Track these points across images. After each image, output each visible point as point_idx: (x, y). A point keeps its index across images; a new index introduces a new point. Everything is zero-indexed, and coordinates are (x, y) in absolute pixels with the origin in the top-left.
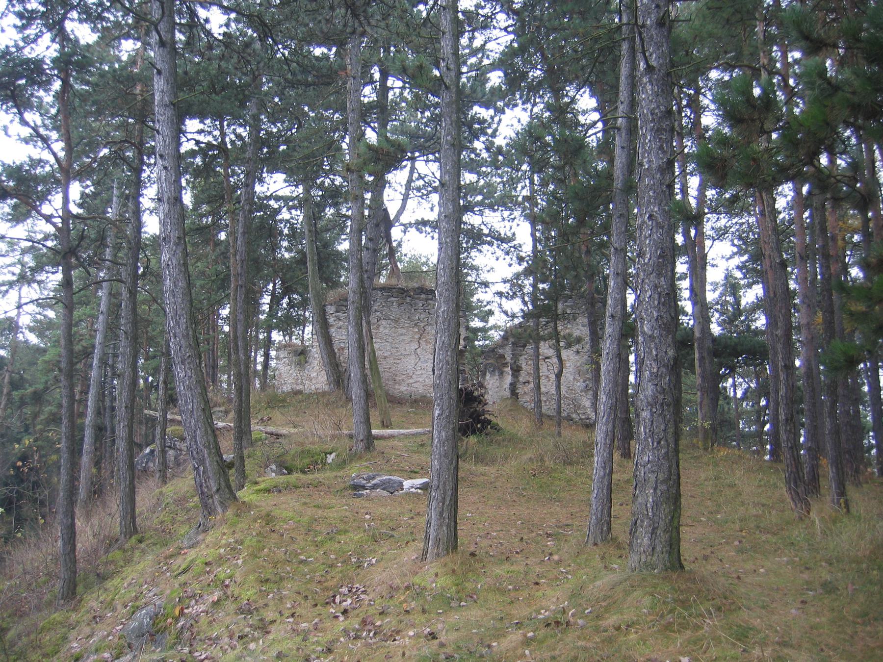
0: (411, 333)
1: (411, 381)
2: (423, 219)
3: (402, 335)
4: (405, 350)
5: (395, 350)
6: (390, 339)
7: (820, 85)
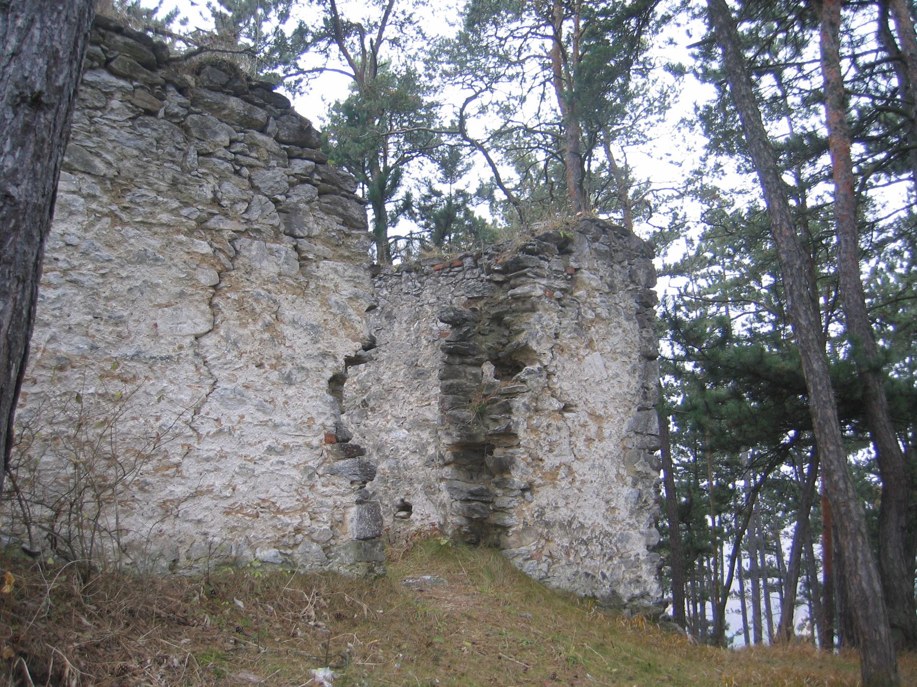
0: (180, 256)
1: (179, 490)
2: (680, 65)
3: (142, 258)
4: (155, 336)
5: (107, 331)
6: (87, 273)
7: (371, 455)
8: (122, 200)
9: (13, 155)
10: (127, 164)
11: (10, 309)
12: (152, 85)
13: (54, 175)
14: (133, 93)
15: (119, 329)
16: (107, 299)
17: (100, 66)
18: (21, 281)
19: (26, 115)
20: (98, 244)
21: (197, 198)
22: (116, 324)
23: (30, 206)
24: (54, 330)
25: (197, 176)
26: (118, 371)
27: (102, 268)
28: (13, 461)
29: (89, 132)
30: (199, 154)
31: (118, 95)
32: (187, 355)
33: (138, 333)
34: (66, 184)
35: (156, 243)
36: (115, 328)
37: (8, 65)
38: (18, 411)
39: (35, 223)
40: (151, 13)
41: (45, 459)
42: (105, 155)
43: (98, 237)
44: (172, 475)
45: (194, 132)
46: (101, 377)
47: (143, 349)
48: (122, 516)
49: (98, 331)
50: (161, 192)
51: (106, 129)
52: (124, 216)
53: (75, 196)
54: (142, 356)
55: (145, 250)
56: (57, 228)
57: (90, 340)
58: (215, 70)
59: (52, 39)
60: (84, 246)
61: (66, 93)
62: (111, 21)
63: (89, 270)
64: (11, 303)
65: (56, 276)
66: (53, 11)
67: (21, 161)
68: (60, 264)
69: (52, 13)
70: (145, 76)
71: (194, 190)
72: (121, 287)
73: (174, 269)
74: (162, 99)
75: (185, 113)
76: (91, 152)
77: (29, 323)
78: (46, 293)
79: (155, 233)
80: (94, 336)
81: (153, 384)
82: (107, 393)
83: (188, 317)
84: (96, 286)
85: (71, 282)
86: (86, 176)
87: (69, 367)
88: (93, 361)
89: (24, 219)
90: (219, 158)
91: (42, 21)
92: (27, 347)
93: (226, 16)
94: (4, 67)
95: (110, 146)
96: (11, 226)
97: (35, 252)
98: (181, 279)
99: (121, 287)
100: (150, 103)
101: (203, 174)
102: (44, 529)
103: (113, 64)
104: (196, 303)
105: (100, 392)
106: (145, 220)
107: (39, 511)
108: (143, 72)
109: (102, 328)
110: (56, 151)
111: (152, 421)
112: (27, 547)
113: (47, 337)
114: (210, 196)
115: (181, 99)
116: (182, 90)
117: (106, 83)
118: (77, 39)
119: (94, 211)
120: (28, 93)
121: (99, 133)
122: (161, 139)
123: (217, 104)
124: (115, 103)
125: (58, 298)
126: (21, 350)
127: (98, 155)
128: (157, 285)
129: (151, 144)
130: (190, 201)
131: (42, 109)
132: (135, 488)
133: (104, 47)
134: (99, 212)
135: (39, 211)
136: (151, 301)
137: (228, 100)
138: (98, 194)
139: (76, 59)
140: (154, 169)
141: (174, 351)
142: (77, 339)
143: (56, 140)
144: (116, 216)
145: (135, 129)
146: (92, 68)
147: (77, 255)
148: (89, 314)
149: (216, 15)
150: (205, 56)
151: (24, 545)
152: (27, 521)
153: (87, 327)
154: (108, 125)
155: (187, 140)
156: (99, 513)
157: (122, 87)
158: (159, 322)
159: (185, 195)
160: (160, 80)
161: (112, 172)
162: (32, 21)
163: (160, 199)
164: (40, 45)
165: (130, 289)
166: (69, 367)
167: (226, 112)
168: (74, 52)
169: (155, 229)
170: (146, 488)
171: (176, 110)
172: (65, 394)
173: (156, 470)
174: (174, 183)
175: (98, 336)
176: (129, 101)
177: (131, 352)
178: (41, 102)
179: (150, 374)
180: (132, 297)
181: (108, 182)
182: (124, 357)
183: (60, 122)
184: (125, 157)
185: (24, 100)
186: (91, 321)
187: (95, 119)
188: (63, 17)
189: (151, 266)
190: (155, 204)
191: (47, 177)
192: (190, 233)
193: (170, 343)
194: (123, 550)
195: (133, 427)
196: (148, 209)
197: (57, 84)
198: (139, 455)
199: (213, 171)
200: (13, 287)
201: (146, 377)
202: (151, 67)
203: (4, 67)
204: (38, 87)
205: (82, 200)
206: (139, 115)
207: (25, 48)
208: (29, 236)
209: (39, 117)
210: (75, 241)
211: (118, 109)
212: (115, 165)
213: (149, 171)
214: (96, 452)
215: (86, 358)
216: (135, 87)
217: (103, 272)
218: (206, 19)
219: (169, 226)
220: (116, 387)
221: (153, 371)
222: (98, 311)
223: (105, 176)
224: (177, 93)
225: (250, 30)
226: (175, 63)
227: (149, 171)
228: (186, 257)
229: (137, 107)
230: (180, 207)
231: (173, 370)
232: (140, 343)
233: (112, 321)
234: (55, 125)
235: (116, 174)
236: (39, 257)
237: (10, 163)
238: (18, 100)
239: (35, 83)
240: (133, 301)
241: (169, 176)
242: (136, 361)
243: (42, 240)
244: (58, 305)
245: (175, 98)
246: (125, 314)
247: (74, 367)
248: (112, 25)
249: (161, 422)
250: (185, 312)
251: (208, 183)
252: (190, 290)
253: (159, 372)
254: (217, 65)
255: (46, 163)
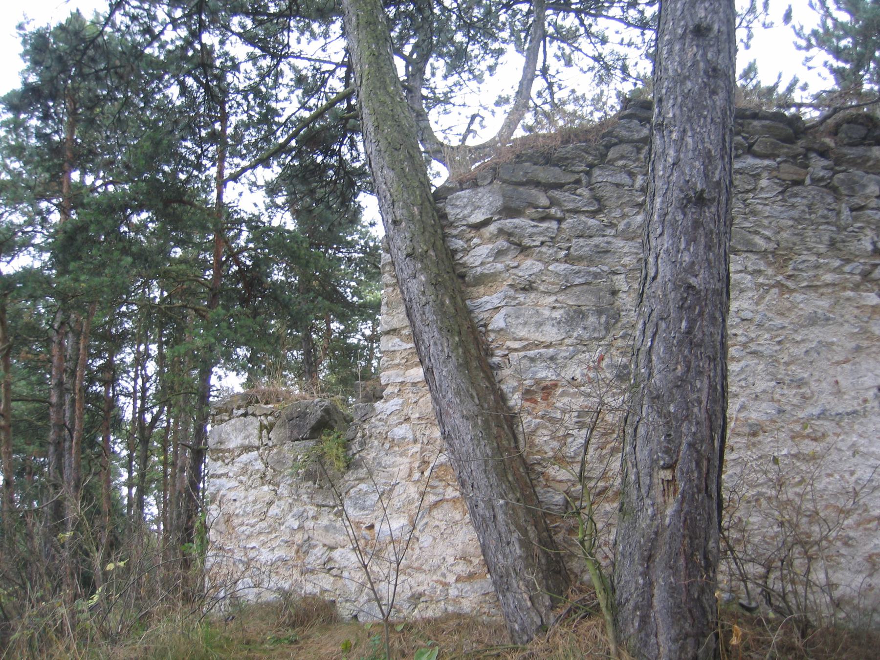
0: (850, 311)
3: (813, 321)
4: (838, 391)
5: (791, 394)
6: (765, 343)
8: (786, 269)
9: (689, 250)
10: (785, 235)
11: (706, 386)
12: (795, 157)
13: (726, 260)
14: (777, 169)
15: (802, 391)
16: (787, 364)
17: (744, 153)
18: (712, 359)
19: (693, 213)
20: (770, 315)
21: (857, 253)
22: (799, 387)
23: (710, 292)
24: (743, 399)
25: (853, 231)
26: (808, 430)
27: (777, 336)
28: (725, 523)
29: (745, 214)
30: (852, 210)
31: (765, 174)
32: (873, 408)
33: (821, 392)
34: (735, 264)
35: (824, 303)
36: (798, 390)
37: (671, 174)
38: (723, 476)
39: (716, 306)
40: (771, 90)
41: (751, 520)
42: (763, 232)
43: (769, 308)
44: (874, 528)
45: (843, 190)
46: (792, 438)
47: (828, 407)
48: (830, 572)
49: (782, 395)
50: (821, 254)
51: (760, 207)
52: (790, 284)
53: (743, 275)
54: (827, 414)
55: (815, 312)
56: (734, 306)
57: (776, 405)
58: (852, 125)
59: (703, 142)
60: (758, 318)
61: (723, 185)
62: (746, 110)
63: (766, 340)
64: (706, 381)
65: (737, 350)
66: (699, 118)
67: (696, 254)
68: (739, 339)
69: (700, 120)
70: (786, 150)
71: (853, 246)
72: (799, 351)
73: (846, 325)
74: (806, 167)
75: (830, 174)
76: (750, 232)
77: (723, 396)
78: (733, 367)
79: (822, 294)
80: (779, 401)
81: (843, 440)
82: (800, 453)
83: (868, 370)
84: (775, 354)
85: (751, 353)
86: (749, 255)
87: (761, 432)
88: (783, 424)
89: (706, 305)
90: (873, 209)
91: (692, 129)
92: (724, 418)
93: (844, 69)
94: (669, 177)
95: (766, 222)
96: (697, 312)
97: (720, 331)
98: (854, 334)
99: (799, 351)
100: (796, 174)
101: (859, 228)
102: (758, 585)
103: (755, 148)
104: (874, 355)
105: (792, 452)
106: (811, 284)
107: (754, 569)
108: (782, 147)
109: (785, 392)
110: (723, 238)
111: (847, 476)
112: (745, 602)
113: (738, 406)
114: (870, 248)
115: (825, 162)
116: (824, 153)
117: (752, 166)
118: (724, 135)
119: (762, 285)
120: (692, 194)
121: (754, 213)
122: (812, 204)
123: (860, 158)
124: (764, 183)
125: (742, 370)
126: (720, 422)
127: (757, 233)
128: (832, 343)
129: (803, 211)
130: (851, 257)
131: (706, 205)
132: (839, 544)
133: (744, 135)
134: (766, 285)
135: (718, 295)
136: (828, 360)
137: (871, 150)
138: (762, 268)
139: (726, 153)
140: (810, 233)
141: (859, 405)
142: (764, 405)
143: (722, 229)
144: (783, 285)
145: (786, 201)
146: (737, 156)
147: (753, 328)
148: (772, 380)
149: (836, 72)
150: (840, 115)
151: (741, 601)
152: (744, 578)
153: (772, 393)
154: (760, 204)
155: (837, 199)
156: (809, 568)
157: (768, 166)
158: (839, 378)
159: (844, 253)
160: (801, 150)
161: (772, 246)
162: (684, 131)
163: (821, 261)
164: (694, 150)
165: (807, 352)
166: (761, 432)
167: (871, 163)
168: (724, 148)
169: (821, 290)
170: (850, 542)
171: (821, 174)
172: (761, 457)
173: (858, 524)
174: (832, 243)
175: (783, 400)
176: (776, 177)
177: (816, 411)
178: (704, 199)
179: (838, 431)
180: (810, 359)
181: (770, 256)
182: (811, 417)
183: (722, 212)
184: (781, 229)
185: (689, 201)
186: (774, 387)
187: (748, 201)
188: (709, 120)
189: (823, 326)
190: (817, 267)
191: (720, 263)
192: (856, 287)
193: (854, 398)
194: (837, 604)
195: (829, 483)
196: (811, 273)
197: (715, 180)
198: (841, 511)
199: (869, 223)
200: (706, 366)
201: (835, 434)
202: (790, 140)
203: (669, 177)
204: (699, 187)
205: (749, 277)
206: (787, 188)
207: (682, 156)
208: (713, 318)
209: (705, 212)
210: (749, 315)
211: (767, 187)
212: (773, 239)
213: (806, 237)
214: (798, 511)
215: (775, 422)
216: (779, 163)
217: (778, 339)
218: (825, 79)
219: (834, 285)
220: (808, 447)
221: (840, 427)
222: (779, 376)
223: (766, 250)
224: (819, 158)
225: (872, 75)
226: (812, 130)
227: (806, 237)
228: (856, 312)
229: (784, 181)
230: (842, 265)
231: (861, 423)
232: (823, 401)
233: (794, 384)
234: (719, 216)
235: (776, 246)
236: (724, 336)
237: (687, 258)
238: (685, 202)
239: (696, 183)
240: (811, 362)
241: (826, 238)
242: (823, 419)
243: (724, 320)
244: (743, 376)
245: (818, 163)
246: (806, 376)
247: (765, 432)
248: (748, 113)
249: (856, 476)
250: (864, 366)
251: (866, 235)
252: (865, 344)
253: (847, 428)
254: (852, 121)
255: (717, 251)
